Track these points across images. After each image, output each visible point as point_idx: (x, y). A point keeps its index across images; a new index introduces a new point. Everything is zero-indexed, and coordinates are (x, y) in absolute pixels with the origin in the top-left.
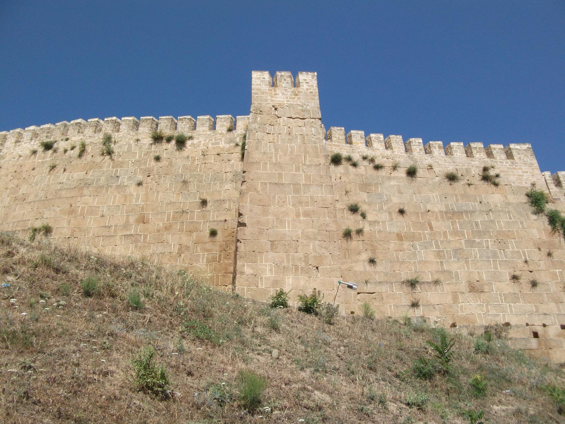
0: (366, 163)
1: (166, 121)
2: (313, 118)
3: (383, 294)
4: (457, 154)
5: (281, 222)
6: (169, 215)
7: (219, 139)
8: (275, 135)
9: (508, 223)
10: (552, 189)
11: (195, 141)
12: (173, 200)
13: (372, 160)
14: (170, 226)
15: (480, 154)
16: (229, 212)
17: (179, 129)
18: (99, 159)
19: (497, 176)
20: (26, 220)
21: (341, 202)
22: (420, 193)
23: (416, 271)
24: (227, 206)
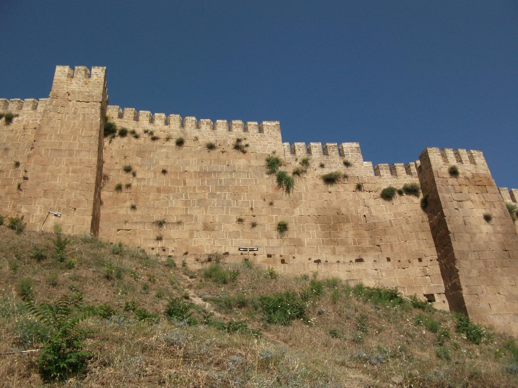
0: (146, 135)
2: (95, 102)
3: (137, 231)
4: (219, 129)
5: (54, 177)
7: (38, 117)
8: (64, 114)
9: (245, 181)
10: (287, 155)
11: (20, 118)
13: (151, 133)
15: (237, 129)
17: (10, 109)
19: (247, 146)
21: (119, 164)
22: (183, 158)
23: (165, 215)
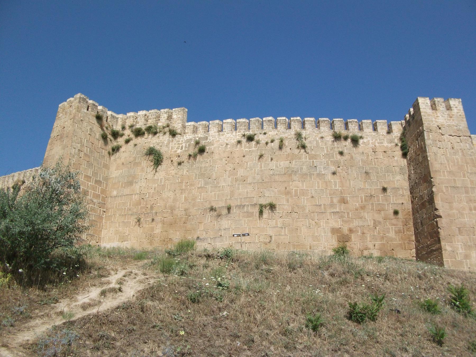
1: (339, 123)
6: (362, 198)
7: (382, 140)
11: (365, 140)
12: (362, 187)
14: (364, 206)
16: (403, 197)
18: (296, 151)
20: (251, 197)
24: (401, 192)
